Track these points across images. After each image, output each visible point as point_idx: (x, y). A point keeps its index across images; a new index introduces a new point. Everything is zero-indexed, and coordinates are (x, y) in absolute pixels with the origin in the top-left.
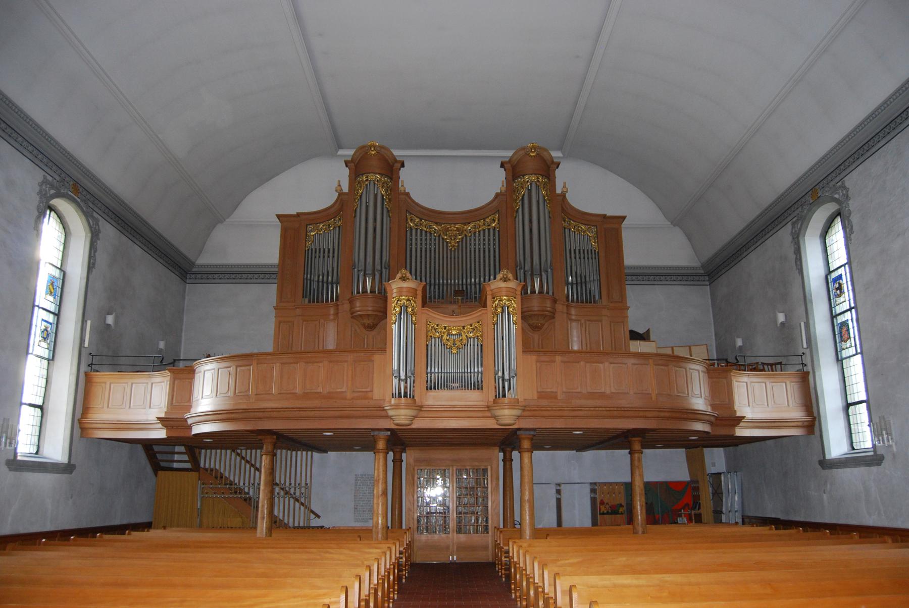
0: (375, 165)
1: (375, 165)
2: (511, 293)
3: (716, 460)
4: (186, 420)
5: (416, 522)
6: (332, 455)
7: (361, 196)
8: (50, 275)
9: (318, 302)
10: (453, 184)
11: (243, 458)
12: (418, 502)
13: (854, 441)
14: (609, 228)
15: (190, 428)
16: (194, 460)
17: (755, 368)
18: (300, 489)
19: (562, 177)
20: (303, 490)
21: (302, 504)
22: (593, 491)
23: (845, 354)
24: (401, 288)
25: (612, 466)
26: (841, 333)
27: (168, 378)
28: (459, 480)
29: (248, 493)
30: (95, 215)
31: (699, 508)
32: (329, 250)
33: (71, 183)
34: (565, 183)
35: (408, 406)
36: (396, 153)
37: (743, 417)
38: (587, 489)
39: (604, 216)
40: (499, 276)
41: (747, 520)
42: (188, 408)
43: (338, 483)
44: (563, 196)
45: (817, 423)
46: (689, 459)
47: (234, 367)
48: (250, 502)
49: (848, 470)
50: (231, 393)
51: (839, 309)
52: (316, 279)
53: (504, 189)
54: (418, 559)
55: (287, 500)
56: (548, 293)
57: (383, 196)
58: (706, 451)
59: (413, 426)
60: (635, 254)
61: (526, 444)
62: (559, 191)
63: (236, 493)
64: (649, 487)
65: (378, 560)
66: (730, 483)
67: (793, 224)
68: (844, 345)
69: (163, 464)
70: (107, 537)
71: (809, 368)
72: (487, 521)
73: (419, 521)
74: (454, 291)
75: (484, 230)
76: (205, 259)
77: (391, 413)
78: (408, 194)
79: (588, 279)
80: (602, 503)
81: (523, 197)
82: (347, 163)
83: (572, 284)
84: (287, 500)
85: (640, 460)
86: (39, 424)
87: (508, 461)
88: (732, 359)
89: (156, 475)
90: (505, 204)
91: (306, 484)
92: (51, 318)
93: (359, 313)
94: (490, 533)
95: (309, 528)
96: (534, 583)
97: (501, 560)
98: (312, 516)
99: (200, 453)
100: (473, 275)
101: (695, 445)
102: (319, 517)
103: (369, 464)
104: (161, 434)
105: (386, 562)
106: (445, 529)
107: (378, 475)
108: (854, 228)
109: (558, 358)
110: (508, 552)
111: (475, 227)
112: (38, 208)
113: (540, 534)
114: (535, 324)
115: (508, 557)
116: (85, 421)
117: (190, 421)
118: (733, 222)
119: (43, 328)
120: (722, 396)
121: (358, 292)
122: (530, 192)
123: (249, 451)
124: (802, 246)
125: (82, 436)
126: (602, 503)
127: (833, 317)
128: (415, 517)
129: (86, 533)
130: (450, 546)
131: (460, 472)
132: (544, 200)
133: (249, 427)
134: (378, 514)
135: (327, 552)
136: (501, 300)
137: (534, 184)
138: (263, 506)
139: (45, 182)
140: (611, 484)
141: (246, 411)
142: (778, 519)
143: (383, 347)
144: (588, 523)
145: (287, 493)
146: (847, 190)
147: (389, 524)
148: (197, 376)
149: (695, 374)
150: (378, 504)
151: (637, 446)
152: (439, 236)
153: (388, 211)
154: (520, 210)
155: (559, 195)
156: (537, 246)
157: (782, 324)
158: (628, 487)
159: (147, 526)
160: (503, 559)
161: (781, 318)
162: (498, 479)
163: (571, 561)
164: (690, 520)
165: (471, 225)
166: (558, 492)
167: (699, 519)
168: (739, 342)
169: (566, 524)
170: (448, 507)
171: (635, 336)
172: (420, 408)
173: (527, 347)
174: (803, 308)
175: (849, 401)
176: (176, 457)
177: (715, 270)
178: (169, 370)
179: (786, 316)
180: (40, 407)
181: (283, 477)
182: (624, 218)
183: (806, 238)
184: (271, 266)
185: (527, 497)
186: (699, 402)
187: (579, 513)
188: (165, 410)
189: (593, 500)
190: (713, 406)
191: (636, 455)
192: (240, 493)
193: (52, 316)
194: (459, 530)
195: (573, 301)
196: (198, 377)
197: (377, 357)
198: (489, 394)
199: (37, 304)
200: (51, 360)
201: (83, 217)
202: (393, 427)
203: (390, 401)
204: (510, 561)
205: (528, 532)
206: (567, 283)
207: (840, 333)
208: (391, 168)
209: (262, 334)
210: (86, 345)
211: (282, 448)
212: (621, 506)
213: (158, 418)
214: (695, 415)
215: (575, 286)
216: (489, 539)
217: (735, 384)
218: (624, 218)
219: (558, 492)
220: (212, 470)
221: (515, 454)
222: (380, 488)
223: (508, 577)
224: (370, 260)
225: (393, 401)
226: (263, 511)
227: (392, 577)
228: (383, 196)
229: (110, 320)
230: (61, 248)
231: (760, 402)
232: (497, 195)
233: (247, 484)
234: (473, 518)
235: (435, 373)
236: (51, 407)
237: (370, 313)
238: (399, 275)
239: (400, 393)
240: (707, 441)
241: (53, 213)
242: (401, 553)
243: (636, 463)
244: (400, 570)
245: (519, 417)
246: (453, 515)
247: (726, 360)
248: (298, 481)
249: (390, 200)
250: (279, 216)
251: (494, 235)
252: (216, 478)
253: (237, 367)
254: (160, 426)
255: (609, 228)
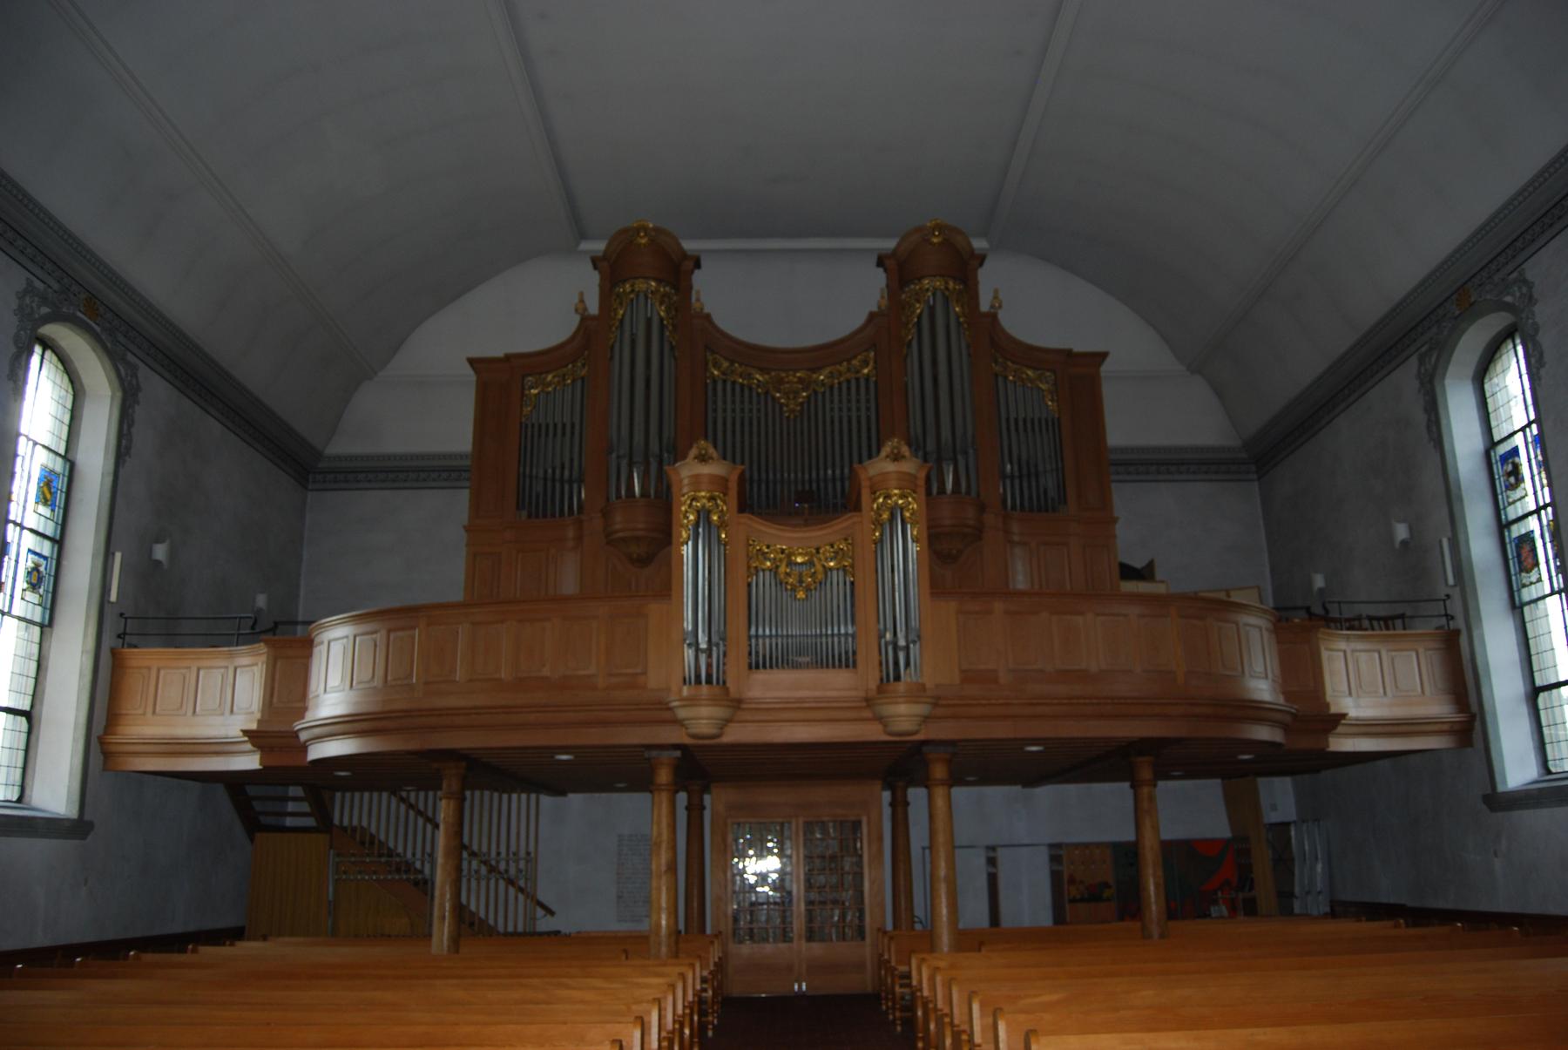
0: (650, 265)
1: (650, 265)
2: (907, 484)
3: (1279, 798)
4: (296, 734)
5: (730, 921)
6: (575, 799)
7: (622, 321)
8: (44, 468)
9: (545, 516)
10: (790, 301)
11: (411, 806)
12: (734, 883)
13: (1550, 757)
14: (1078, 375)
15: (304, 748)
16: (322, 811)
17: (1353, 624)
18: (517, 861)
19: (992, 280)
20: (522, 865)
21: (521, 890)
22: (1055, 859)
23: (1527, 594)
24: (698, 476)
25: (1096, 813)
26: (1519, 556)
27: (264, 658)
28: (808, 841)
29: (421, 872)
30: (130, 357)
31: (1251, 889)
32: (564, 426)
33: (83, 296)
34: (996, 291)
35: (713, 701)
36: (689, 245)
37: (1344, 716)
38: (1043, 857)
39: (1069, 354)
40: (886, 450)
41: (1338, 910)
42: (301, 712)
43: (585, 850)
44: (993, 317)
45: (1477, 724)
46: (1231, 801)
47: (384, 632)
48: (424, 886)
49: (1545, 812)
50: (378, 682)
51: (1513, 512)
52: (541, 474)
53: (885, 303)
54: (737, 990)
55: (492, 882)
56: (968, 493)
57: (662, 320)
58: (1262, 782)
59: (726, 739)
60: (1124, 427)
61: (939, 771)
62: (984, 307)
63: (398, 870)
64: (1168, 848)
65: (659, 1002)
66: (1303, 841)
67: (1421, 362)
68: (1525, 577)
69: (264, 820)
70: (148, 957)
71: (1460, 623)
72: (861, 917)
73: (736, 920)
74: (797, 484)
75: (848, 381)
76: (342, 446)
77: (682, 713)
78: (708, 317)
79: (1041, 468)
80: (1072, 881)
81: (919, 323)
82: (596, 262)
83: (1012, 477)
84: (492, 882)
85: (1152, 799)
86: (22, 746)
87: (900, 806)
88: (1318, 610)
89: (252, 840)
90: (884, 332)
91: (528, 854)
92: (46, 548)
93: (620, 535)
94: (868, 940)
95: (534, 934)
96: (936, 1009)
97: (893, 993)
98: (540, 912)
99: (333, 799)
100: (829, 463)
101: (1236, 767)
102: (550, 912)
103: (646, 816)
104: (250, 762)
105: (675, 1005)
106: (785, 936)
107: (659, 834)
108: (1547, 357)
109: (998, 606)
110: (908, 976)
111: (831, 375)
112: (17, 339)
113: (968, 941)
114: (950, 554)
115: (909, 985)
116: (111, 739)
117: (303, 736)
118: (1302, 363)
119: (30, 564)
120: (1302, 675)
121: (619, 496)
122: (932, 309)
123: (422, 794)
124: (1440, 399)
125: (105, 769)
126: (1072, 881)
127: (1502, 526)
128: (730, 912)
129: (107, 953)
130: (796, 966)
131: (809, 827)
132: (959, 324)
133: (413, 744)
134: (660, 908)
135: (568, 987)
136: (888, 497)
137: (939, 294)
138: (443, 895)
139: (29, 290)
140: (1087, 846)
141: (407, 713)
142: (1403, 906)
143: (666, 588)
144: (1045, 919)
145: (492, 869)
146: (1530, 285)
147: (681, 926)
148: (316, 650)
149: (1255, 635)
150: (659, 889)
151: (1146, 774)
152: (767, 393)
153: (672, 348)
154: (915, 343)
155: (987, 315)
156: (952, 405)
157: (1404, 543)
158: (1127, 855)
159: (234, 934)
160: (898, 989)
161: (1401, 532)
162: (880, 839)
163: (1046, 998)
164: (1233, 911)
165: (827, 371)
166: (992, 862)
167: (1251, 909)
168: (1319, 582)
169: (1007, 921)
170: (790, 893)
171: (1128, 572)
172: (737, 704)
173: (937, 589)
174: (1445, 511)
175: (1538, 683)
176: (291, 807)
177: (1268, 453)
178: (266, 642)
179: (1411, 529)
180: (27, 715)
181: (485, 841)
182: (1103, 356)
183: (1448, 382)
184: (462, 456)
185: (942, 871)
186: (1262, 688)
187: (1029, 902)
188: (258, 716)
189: (1056, 877)
190: (1288, 695)
191: (1145, 790)
192: (407, 872)
193: (47, 544)
194: (811, 936)
195: (1014, 507)
196: (319, 653)
197: (655, 609)
198: (867, 676)
199: (12, 517)
200: (46, 626)
201: (106, 359)
202: (687, 741)
203: (680, 690)
204: (913, 994)
205: (945, 939)
206: (1003, 476)
207: (1518, 556)
208: (677, 269)
209: (446, 577)
210: (113, 597)
211: (473, 789)
212: (1106, 885)
213: (245, 732)
214: (1254, 711)
215: (1017, 482)
216: (866, 951)
217: (1325, 655)
218: (1103, 356)
219: (992, 862)
220: (354, 830)
221: (916, 795)
222: (664, 857)
223: (910, 1023)
224: (639, 437)
225: (685, 691)
226: (442, 906)
227: (687, 1031)
228: (662, 320)
229: (160, 552)
230: (67, 419)
231: (1371, 687)
232: (872, 316)
233: (419, 855)
234: (837, 912)
235: (764, 636)
236: (46, 712)
237: (640, 533)
238: (693, 452)
239: (698, 677)
240: (1273, 761)
241: (48, 354)
242: (704, 980)
243: (1145, 805)
244: (702, 1014)
245: (926, 719)
246: (799, 907)
247: (1308, 609)
248: (513, 849)
249: (674, 326)
250: (472, 361)
251: (867, 389)
252: (363, 843)
253: (389, 631)
254: (249, 746)
255: (1078, 375)
